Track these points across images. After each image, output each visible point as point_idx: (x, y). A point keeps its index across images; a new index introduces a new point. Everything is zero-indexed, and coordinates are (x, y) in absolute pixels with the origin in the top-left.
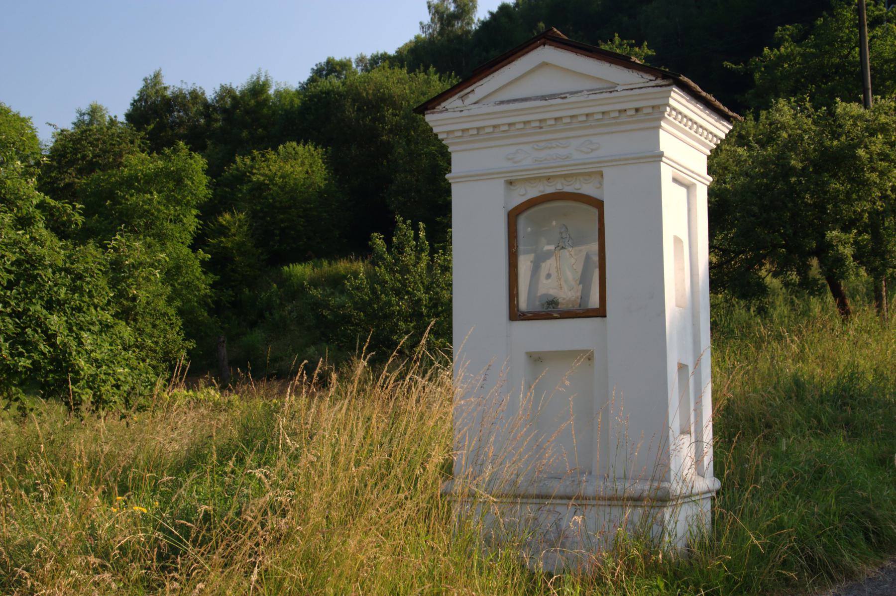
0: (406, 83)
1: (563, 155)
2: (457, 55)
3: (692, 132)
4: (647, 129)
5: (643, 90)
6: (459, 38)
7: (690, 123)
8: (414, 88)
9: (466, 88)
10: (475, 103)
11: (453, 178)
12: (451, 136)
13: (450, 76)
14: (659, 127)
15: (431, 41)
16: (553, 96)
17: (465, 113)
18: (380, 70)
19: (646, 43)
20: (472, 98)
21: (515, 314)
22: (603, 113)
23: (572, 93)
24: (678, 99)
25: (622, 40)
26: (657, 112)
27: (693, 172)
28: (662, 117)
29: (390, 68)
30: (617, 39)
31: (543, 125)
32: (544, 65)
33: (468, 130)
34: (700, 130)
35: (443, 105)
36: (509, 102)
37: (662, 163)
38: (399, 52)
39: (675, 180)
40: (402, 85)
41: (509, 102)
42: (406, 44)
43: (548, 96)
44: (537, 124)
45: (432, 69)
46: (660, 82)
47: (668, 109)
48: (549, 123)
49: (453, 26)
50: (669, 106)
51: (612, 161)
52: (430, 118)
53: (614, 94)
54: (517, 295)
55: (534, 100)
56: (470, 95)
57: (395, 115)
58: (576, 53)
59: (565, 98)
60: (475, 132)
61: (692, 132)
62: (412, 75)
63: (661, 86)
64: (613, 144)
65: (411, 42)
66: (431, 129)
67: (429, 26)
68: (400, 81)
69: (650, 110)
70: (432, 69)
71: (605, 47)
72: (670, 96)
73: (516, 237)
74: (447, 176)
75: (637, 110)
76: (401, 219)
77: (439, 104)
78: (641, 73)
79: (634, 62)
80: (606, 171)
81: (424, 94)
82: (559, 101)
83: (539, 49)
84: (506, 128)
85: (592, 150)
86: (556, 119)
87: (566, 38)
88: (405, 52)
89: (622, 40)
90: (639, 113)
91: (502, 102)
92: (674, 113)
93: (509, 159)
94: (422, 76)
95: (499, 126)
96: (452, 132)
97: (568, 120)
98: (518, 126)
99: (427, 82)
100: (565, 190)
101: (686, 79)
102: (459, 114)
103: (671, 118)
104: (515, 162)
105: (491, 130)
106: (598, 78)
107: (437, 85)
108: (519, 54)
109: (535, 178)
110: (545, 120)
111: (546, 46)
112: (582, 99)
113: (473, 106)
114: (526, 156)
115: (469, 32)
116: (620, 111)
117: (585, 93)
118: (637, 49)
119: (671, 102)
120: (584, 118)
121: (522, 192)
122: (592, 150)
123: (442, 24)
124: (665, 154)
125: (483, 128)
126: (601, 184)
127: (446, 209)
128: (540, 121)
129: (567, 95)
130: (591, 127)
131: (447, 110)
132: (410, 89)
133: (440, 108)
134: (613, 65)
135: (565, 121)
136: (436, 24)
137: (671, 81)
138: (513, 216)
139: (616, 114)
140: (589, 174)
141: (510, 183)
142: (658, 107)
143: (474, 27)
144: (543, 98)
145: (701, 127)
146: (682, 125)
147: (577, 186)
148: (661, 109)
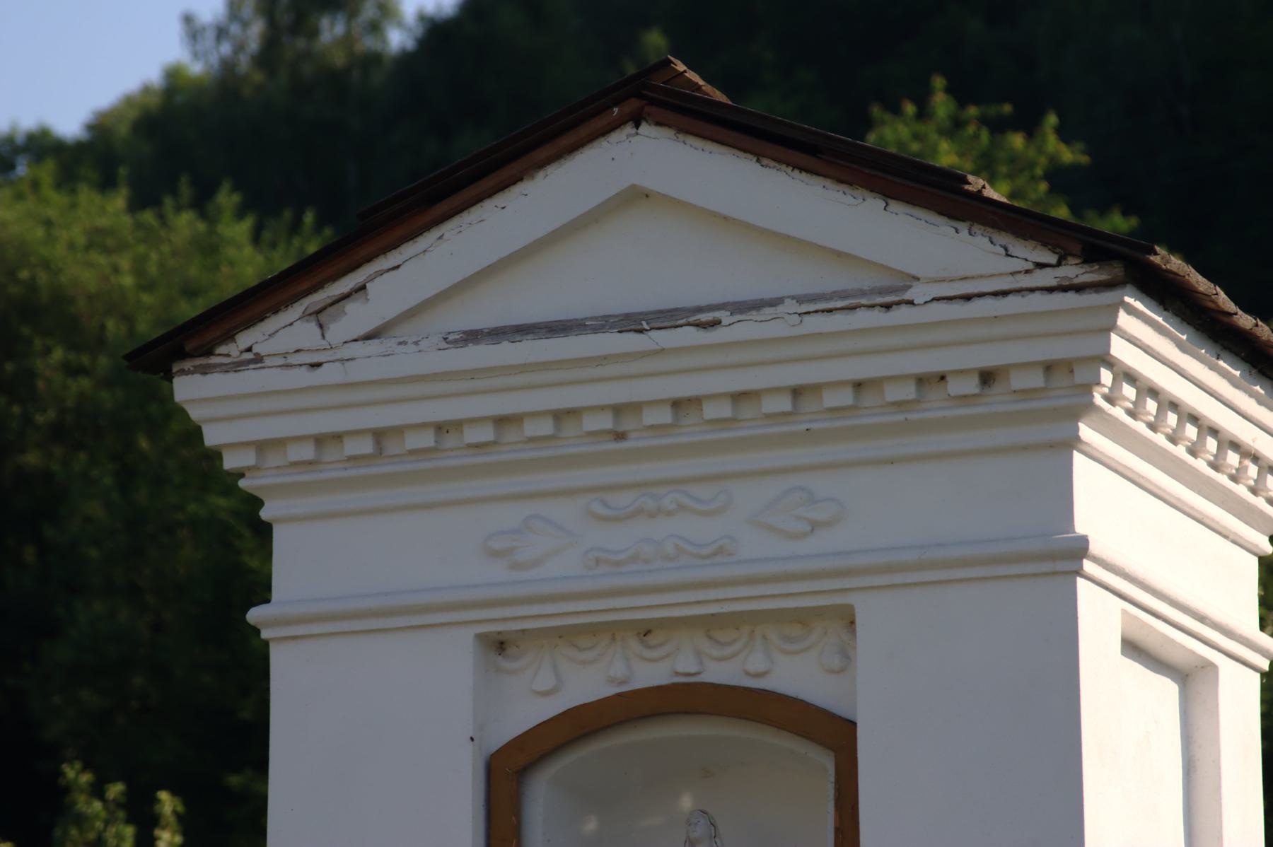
0: (122, 247)
1: (689, 545)
2: (301, 160)
3: (1200, 465)
4: (1026, 448)
6: (334, 81)
7: (1191, 431)
8: (153, 269)
10: (369, 337)
12: (273, 459)
13: (295, 227)
14: (1074, 442)
15: (226, 83)
16: (667, 318)
17: (328, 374)
18: (19, 197)
19: (1052, 120)
20: (358, 317)
22: (858, 385)
23: (741, 308)
24: (1142, 340)
26: (1064, 388)
27: (1202, 619)
28: (1082, 408)
29: (58, 186)
30: (942, 104)
31: (627, 424)
32: (636, 197)
33: (338, 437)
34: (1233, 458)
35: (244, 339)
36: (497, 334)
37: (1081, 583)
38: (100, 128)
39: (1133, 648)
40: (102, 253)
41: (497, 334)
42: (129, 101)
43: (646, 316)
44: (605, 422)
45: (227, 199)
46: (1073, 271)
47: (1106, 376)
49: (314, 33)
50: (1110, 363)
51: (889, 569)
52: (191, 390)
53: (901, 315)
55: (596, 330)
56: (351, 307)
57: (72, 371)
58: (759, 156)
59: (716, 323)
60: (365, 446)
61: (1200, 465)
62: (148, 217)
63: (1079, 288)
64: (890, 504)
65: (146, 90)
66: (195, 433)
67: (221, 33)
68: (98, 240)
69: (1036, 379)
70: (227, 199)
71: (893, 133)
72: (1112, 327)
74: (255, 615)
75: (987, 377)
76: (86, 778)
77: (229, 337)
78: (1003, 238)
79: (978, 196)
80: (867, 609)
81: (190, 292)
82: (689, 336)
83: (615, 136)
84: (485, 434)
85: (815, 526)
86: (676, 404)
87: (719, 96)
88: (123, 130)
90: (997, 388)
91: (472, 337)
92: (1129, 391)
93: (496, 554)
94: (185, 224)
95: (458, 425)
96: (280, 443)
97: (725, 410)
98: (530, 429)
99: (209, 249)
100: (707, 677)
101: (1176, 264)
102: (304, 378)
103: (1118, 412)
104: (516, 566)
106: (839, 254)
107: (246, 259)
108: (540, 154)
109: (593, 630)
110: (635, 407)
111: (644, 128)
112: (776, 329)
114: (559, 541)
115: (373, 60)
116: (921, 381)
117: (790, 306)
118: (1017, 141)
119: (1119, 348)
120: (784, 404)
121: (545, 680)
122: (815, 526)
123: (272, 23)
124: (1094, 548)
125: (399, 431)
126: (846, 655)
127: (248, 742)
128: (618, 410)
129: (723, 315)
130: (810, 437)
131: (259, 359)
132: (139, 270)
134: (895, 206)
135: (710, 411)
136: (245, 25)
137: (1117, 270)
139: (908, 391)
140: (803, 618)
141: (499, 645)
142: (1069, 366)
143: (397, 39)
144: (632, 323)
145: (1235, 446)
146: (1160, 439)
147: (756, 662)
148: (1080, 376)
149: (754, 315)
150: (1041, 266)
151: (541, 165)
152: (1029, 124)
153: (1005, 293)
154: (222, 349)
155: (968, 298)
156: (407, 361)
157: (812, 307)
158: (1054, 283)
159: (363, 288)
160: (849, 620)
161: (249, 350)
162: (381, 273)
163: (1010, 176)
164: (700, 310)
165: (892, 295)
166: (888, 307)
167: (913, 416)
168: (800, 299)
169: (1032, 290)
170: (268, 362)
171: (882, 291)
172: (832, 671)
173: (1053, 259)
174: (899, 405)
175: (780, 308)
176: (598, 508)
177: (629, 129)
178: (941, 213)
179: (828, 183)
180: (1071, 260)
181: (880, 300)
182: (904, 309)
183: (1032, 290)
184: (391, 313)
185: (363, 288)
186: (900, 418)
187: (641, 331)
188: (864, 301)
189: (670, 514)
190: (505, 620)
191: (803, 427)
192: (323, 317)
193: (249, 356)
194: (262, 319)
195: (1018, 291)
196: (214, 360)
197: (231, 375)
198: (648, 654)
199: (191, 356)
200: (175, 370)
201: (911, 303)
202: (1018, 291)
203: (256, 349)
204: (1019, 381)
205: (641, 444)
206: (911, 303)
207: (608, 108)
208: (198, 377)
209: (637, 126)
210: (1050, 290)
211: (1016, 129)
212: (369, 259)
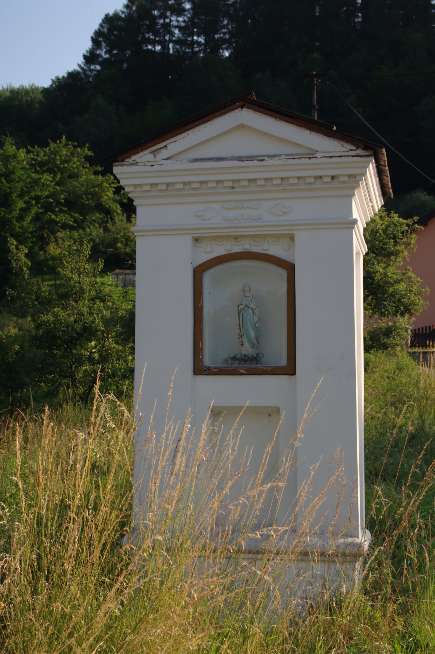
1: (256, 216)
5: (343, 159)
9: (159, 143)
10: (167, 159)
11: (139, 231)
12: (138, 189)
16: (250, 158)
19: (88, 145)
20: (165, 154)
21: (199, 369)
22: (299, 178)
23: (271, 156)
25: (68, 141)
31: (236, 185)
32: (242, 126)
33: (156, 185)
35: (133, 158)
36: (203, 160)
41: (203, 160)
44: (230, 184)
46: (360, 152)
48: (242, 183)
51: (305, 225)
53: (313, 161)
54: (202, 350)
56: (163, 151)
58: (276, 118)
59: (263, 160)
60: (164, 187)
63: (361, 156)
64: (303, 208)
73: (201, 293)
74: (397, 215)
75: (333, 178)
77: (129, 157)
78: (342, 142)
80: (299, 236)
82: (256, 163)
83: (236, 111)
85: (285, 213)
89: (68, 141)
91: (196, 160)
93: (198, 217)
96: (140, 185)
97: (263, 183)
98: (210, 185)
102: (149, 168)
105: (181, 186)
109: (222, 237)
110: (238, 181)
111: (244, 109)
112: (280, 162)
113: (165, 162)
114: (216, 214)
118: (79, 150)
121: (209, 249)
122: (285, 213)
128: (233, 181)
129: (266, 158)
131: (137, 163)
133: (130, 160)
134: (313, 133)
135: (242, 183)
137: (371, 152)
138: (199, 272)
142: (355, 176)
144: (240, 159)
147: (266, 247)
148: (358, 178)
149: (274, 158)
150: (351, 150)
151: (216, 117)
152: (81, 146)
153: (341, 156)
154: (127, 160)
155: (331, 157)
156: (178, 166)
157: (289, 157)
158: (355, 154)
159: (166, 146)
160: (292, 238)
161: (134, 161)
162: (171, 143)
163: (78, 157)
164: (259, 156)
165: (311, 155)
166: (310, 158)
167: (312, 187)
168: (287, 155)
169: (348, 156)
170: (139, 164)
171: (308, 154)
172: (286, 250)
173: (355, 148)
174: (309, 184)
175: (281, 157)
176: (226, 206)
177: (240, 109)
178: (325, 135)
179: (294, 126)
180: (359, 149)
181: (308, 156)
182: (314, 159)
183: (348, 156)
184: (173, 153)
185: (166, 146)
186: (309, 187)
187: (242, 161)
188: (304, 156)
189: (245, 208)
190: (200, 233)
191: (283, 188)
192: (155, 153)
193: (134, 162)
194: (138, 153)
195: (345, 156)
196: (124, 163)
197: (129, 167)
198: (237, 244)
199: (118, 161)
200: (114, 164)
201: (316, 158)
202: (345, 156)
203: (136, 161)
204: (341, 179)
205: (239, 190)
206: (316, 158)
207: (236, 103)
208: (120, 167)
209: (242, 108)
210: (353, 156)
211: (79, 147)
212: (168, 139)
